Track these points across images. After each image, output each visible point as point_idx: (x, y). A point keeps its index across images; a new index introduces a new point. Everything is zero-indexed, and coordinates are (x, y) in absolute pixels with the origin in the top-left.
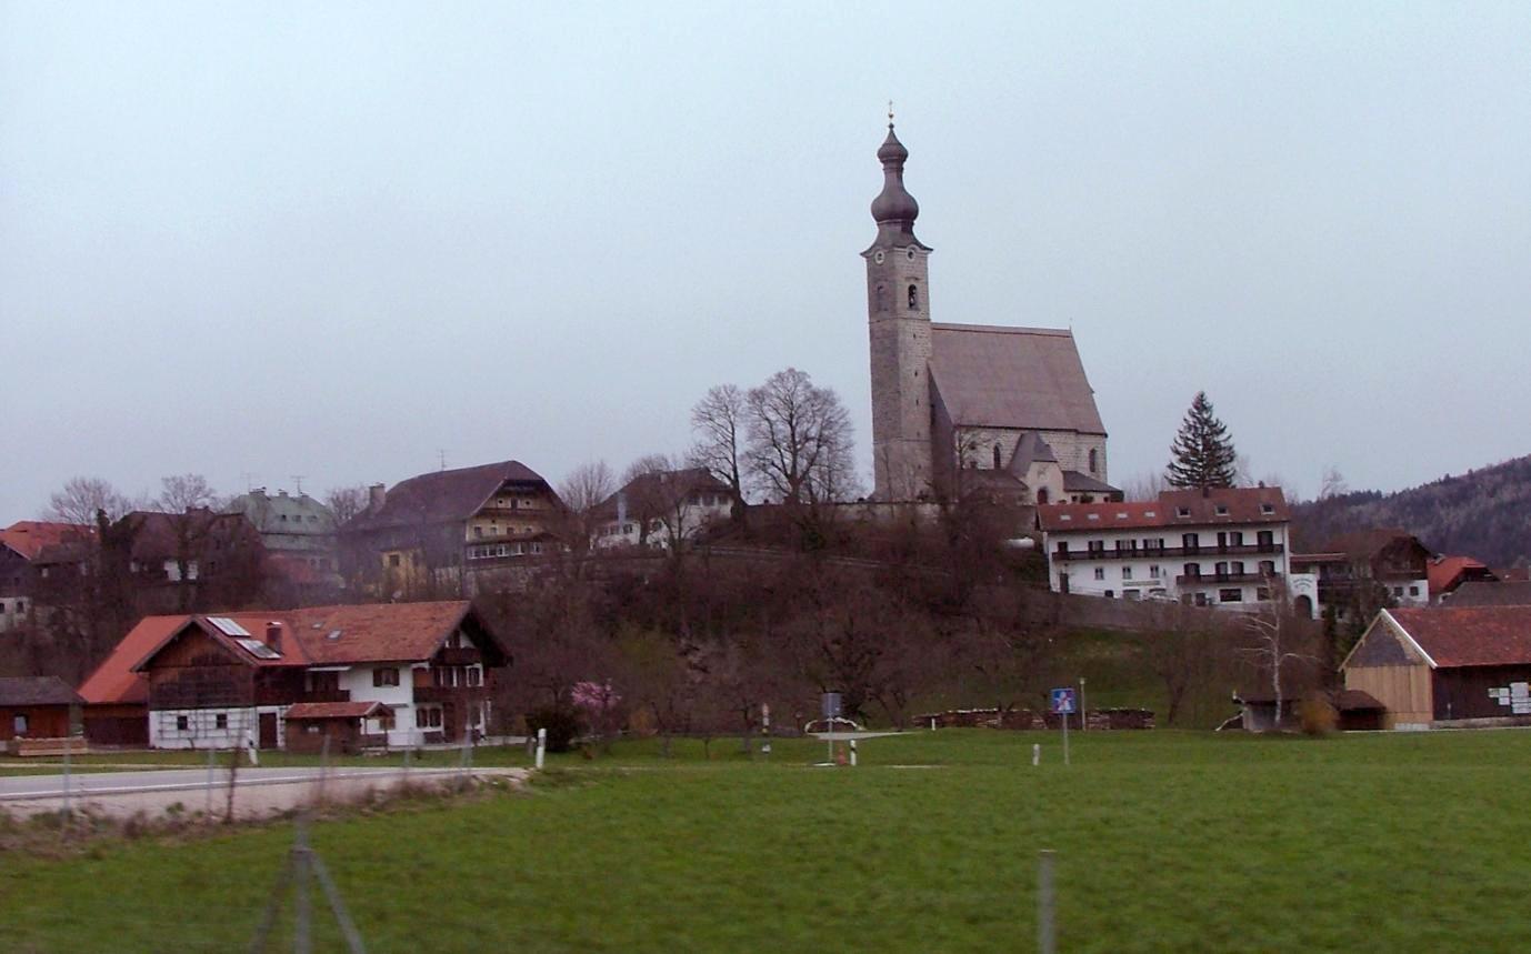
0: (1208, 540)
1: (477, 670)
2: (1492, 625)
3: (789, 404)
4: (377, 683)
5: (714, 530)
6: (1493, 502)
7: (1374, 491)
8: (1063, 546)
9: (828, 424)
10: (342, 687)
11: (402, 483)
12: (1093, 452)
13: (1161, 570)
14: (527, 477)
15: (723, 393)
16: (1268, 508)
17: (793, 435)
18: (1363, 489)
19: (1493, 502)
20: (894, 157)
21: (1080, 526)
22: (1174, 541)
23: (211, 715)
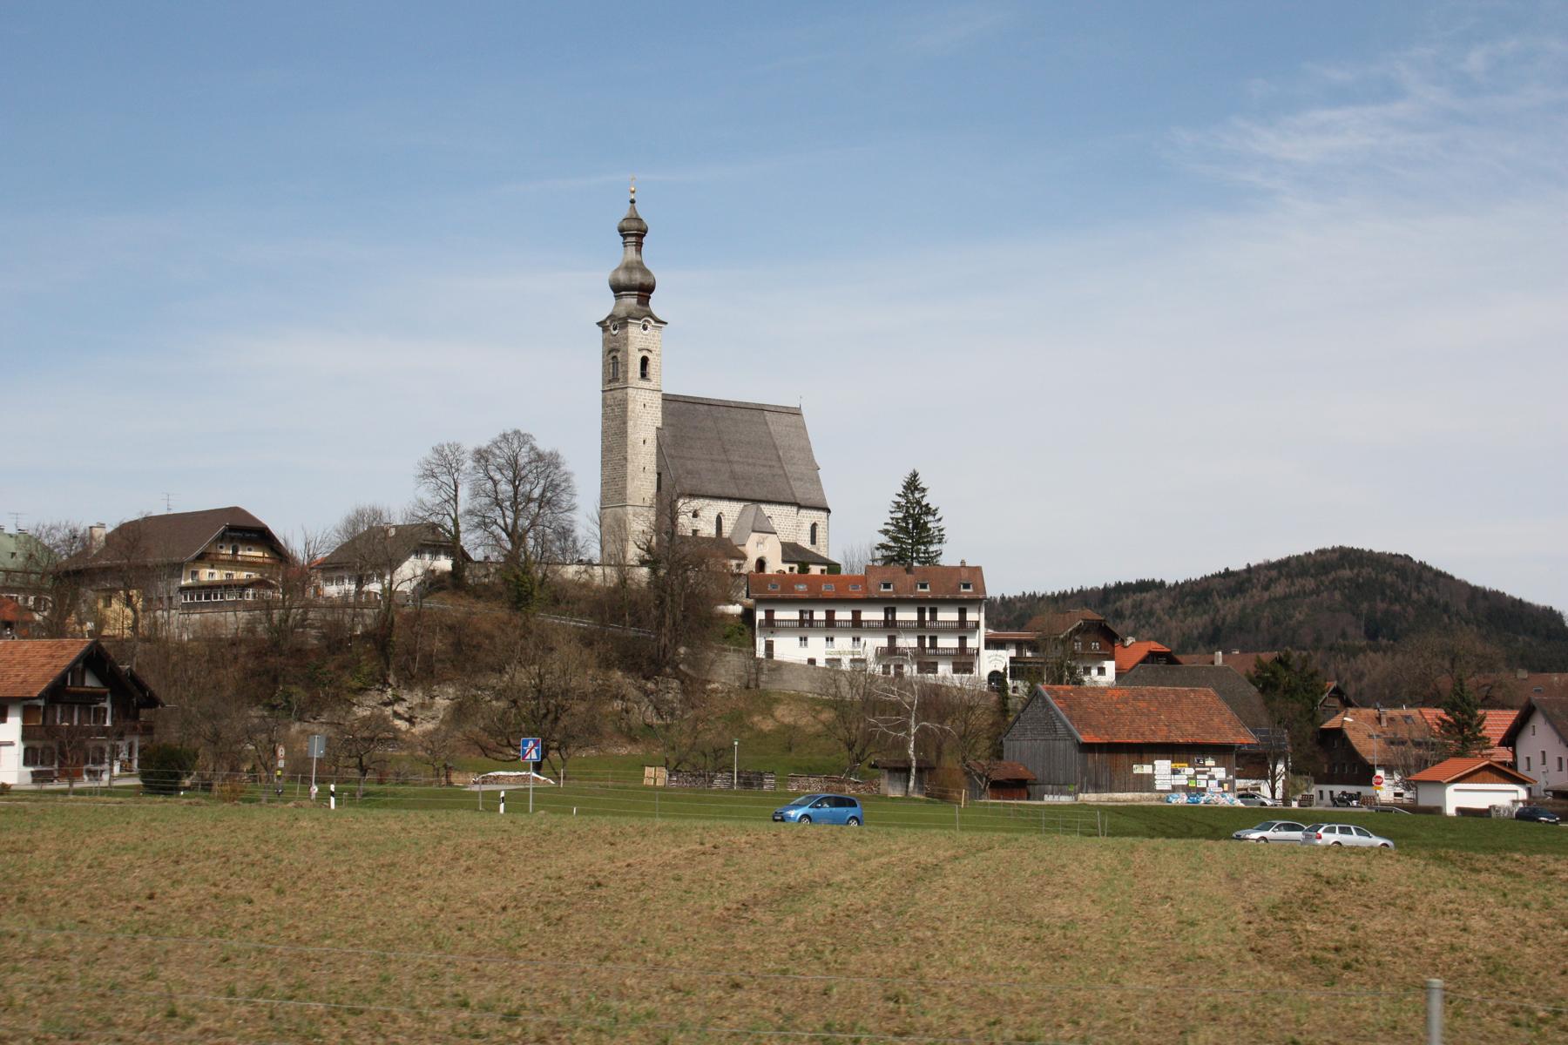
0: (907, 615)
1: (105, 710)
3: (514, 464)
5: (432, 584)
6: (1266, 595)
7: (1158, 580)
9: (553, 486)
12: (814, 526)
15: (447, 451)
16: (967, 586)
17: (516, 494)
18: (1147, 577)
19: (1266, 595)
20: (634, 233)
22: (873, 615)
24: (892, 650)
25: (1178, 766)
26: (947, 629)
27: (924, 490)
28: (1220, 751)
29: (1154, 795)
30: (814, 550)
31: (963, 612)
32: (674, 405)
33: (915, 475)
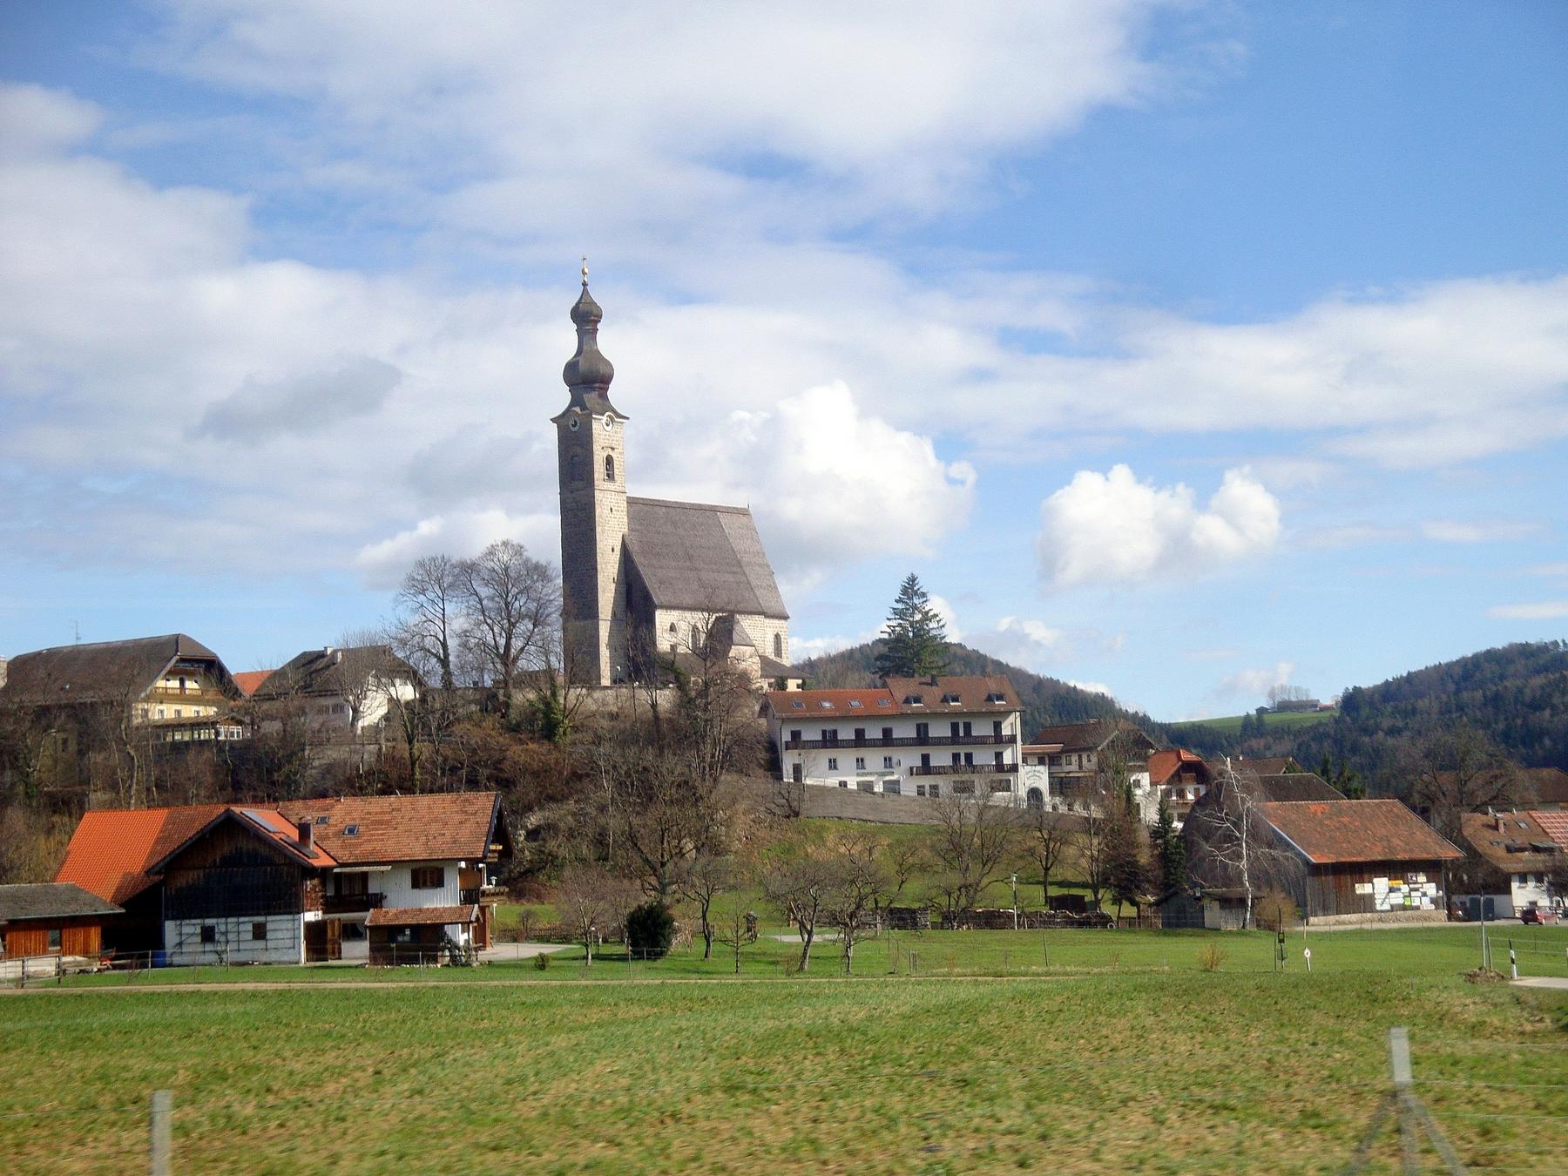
2: (1346, 820)
4: (415, 885)
8: (796, 735)
10: (373, 888)
11: (1524, 652)
12: (777, 637)
13: (894, 761)
14: (198, 655)
20: (586, 318)
21: (815, 714)
22: (905, 731)
23: (246, 924)
24: (926, 768)
25: (1396, 883)
26: (981, 741)
27: (924, 595)
28: (1432, 868)
29: (1376, 915)
30: (778, 660)
31: (182, 682)
32: (637, 507)
33: (912, 580)
